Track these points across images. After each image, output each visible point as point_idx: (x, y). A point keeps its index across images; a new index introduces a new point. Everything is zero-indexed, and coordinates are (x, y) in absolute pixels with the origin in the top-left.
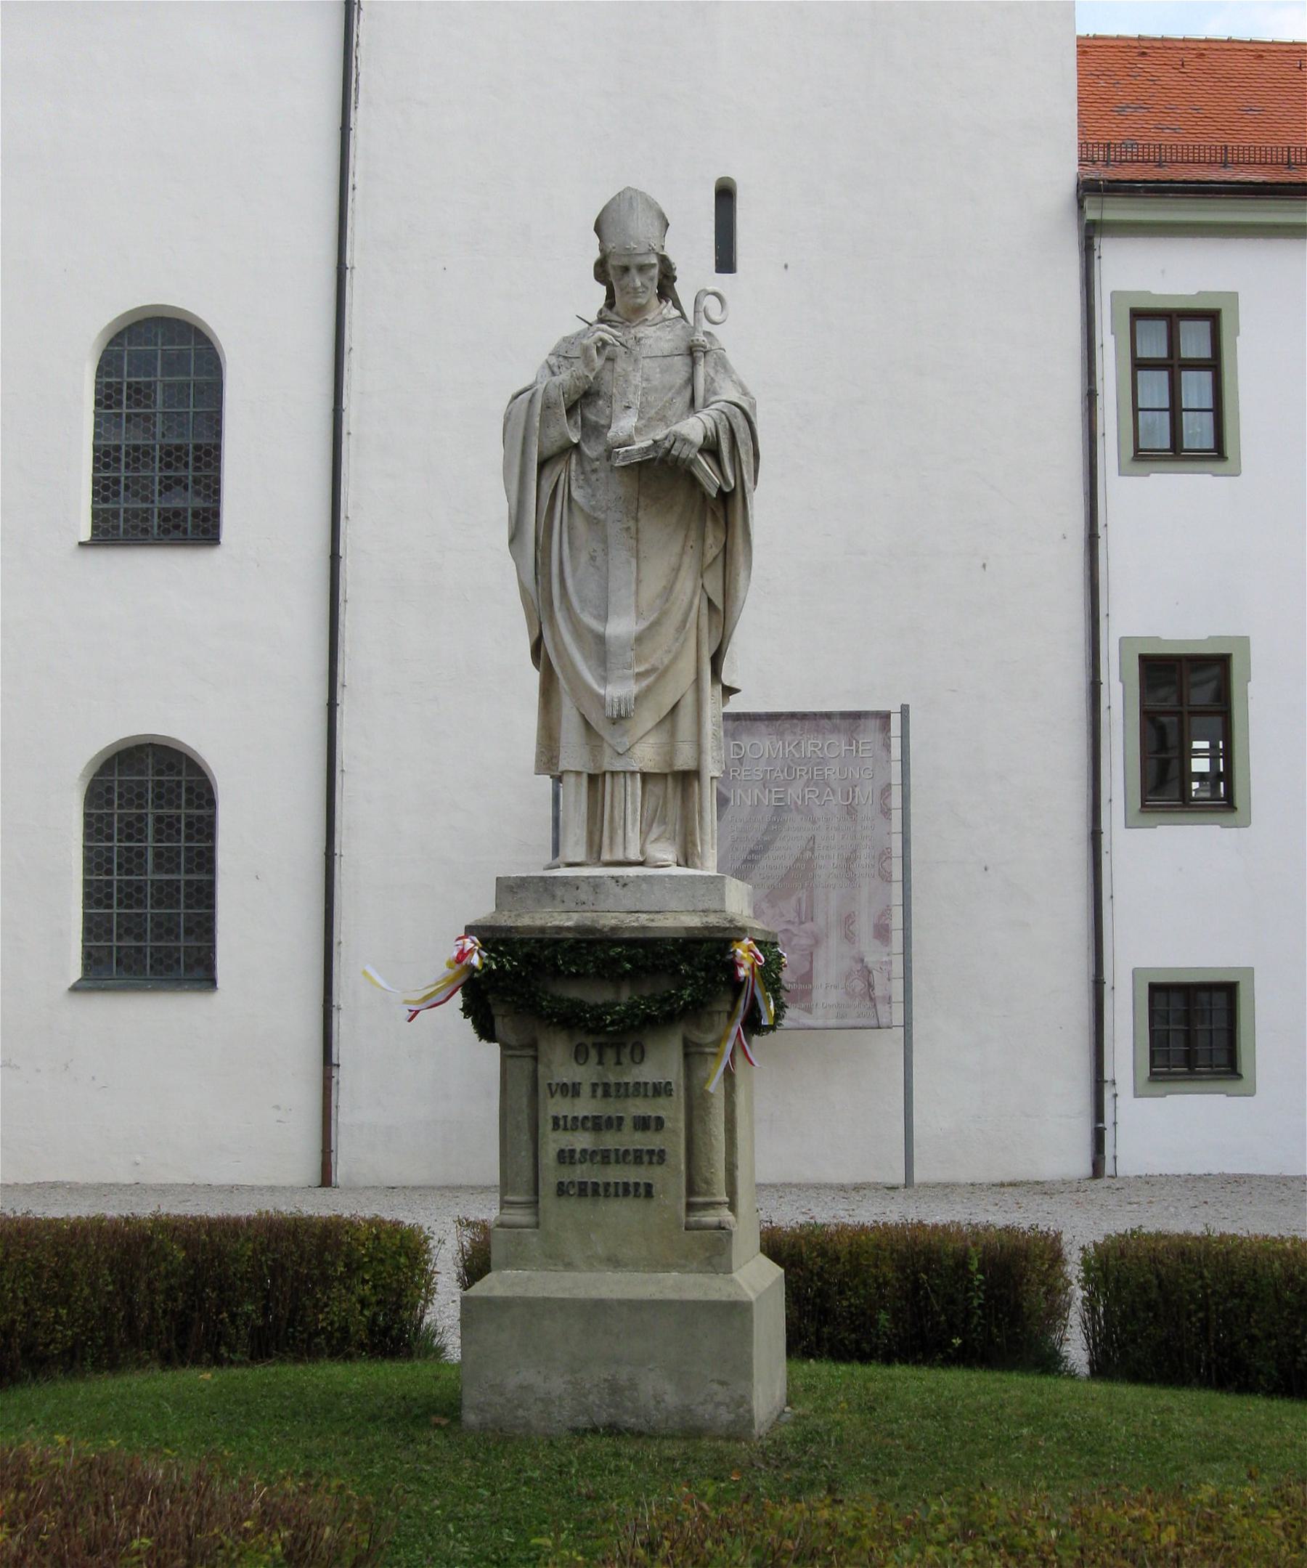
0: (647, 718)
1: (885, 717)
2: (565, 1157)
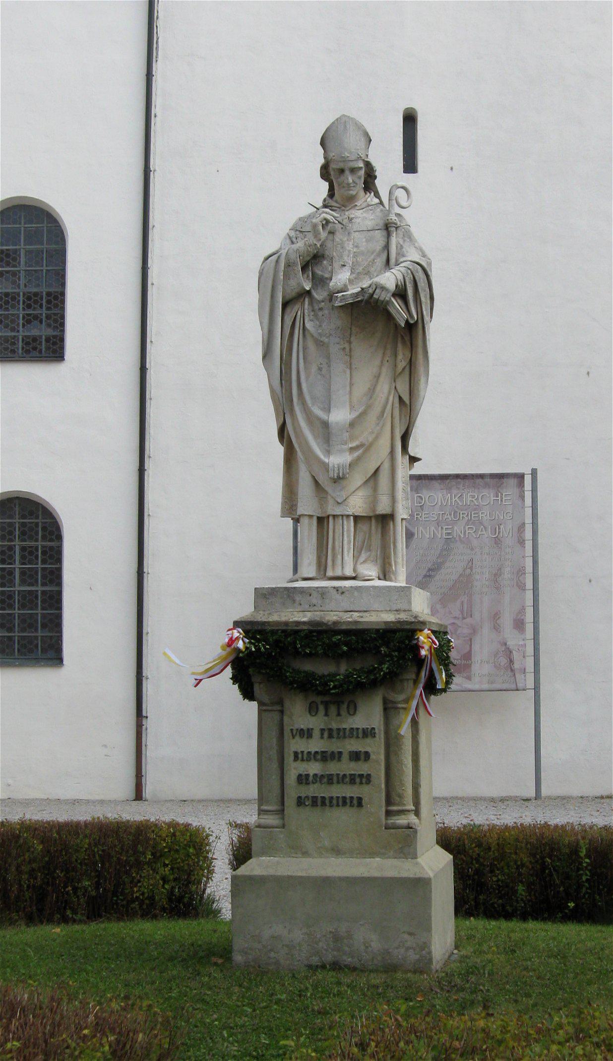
0: (357, 479)
1: (521, 477)
2: (303, 779)
